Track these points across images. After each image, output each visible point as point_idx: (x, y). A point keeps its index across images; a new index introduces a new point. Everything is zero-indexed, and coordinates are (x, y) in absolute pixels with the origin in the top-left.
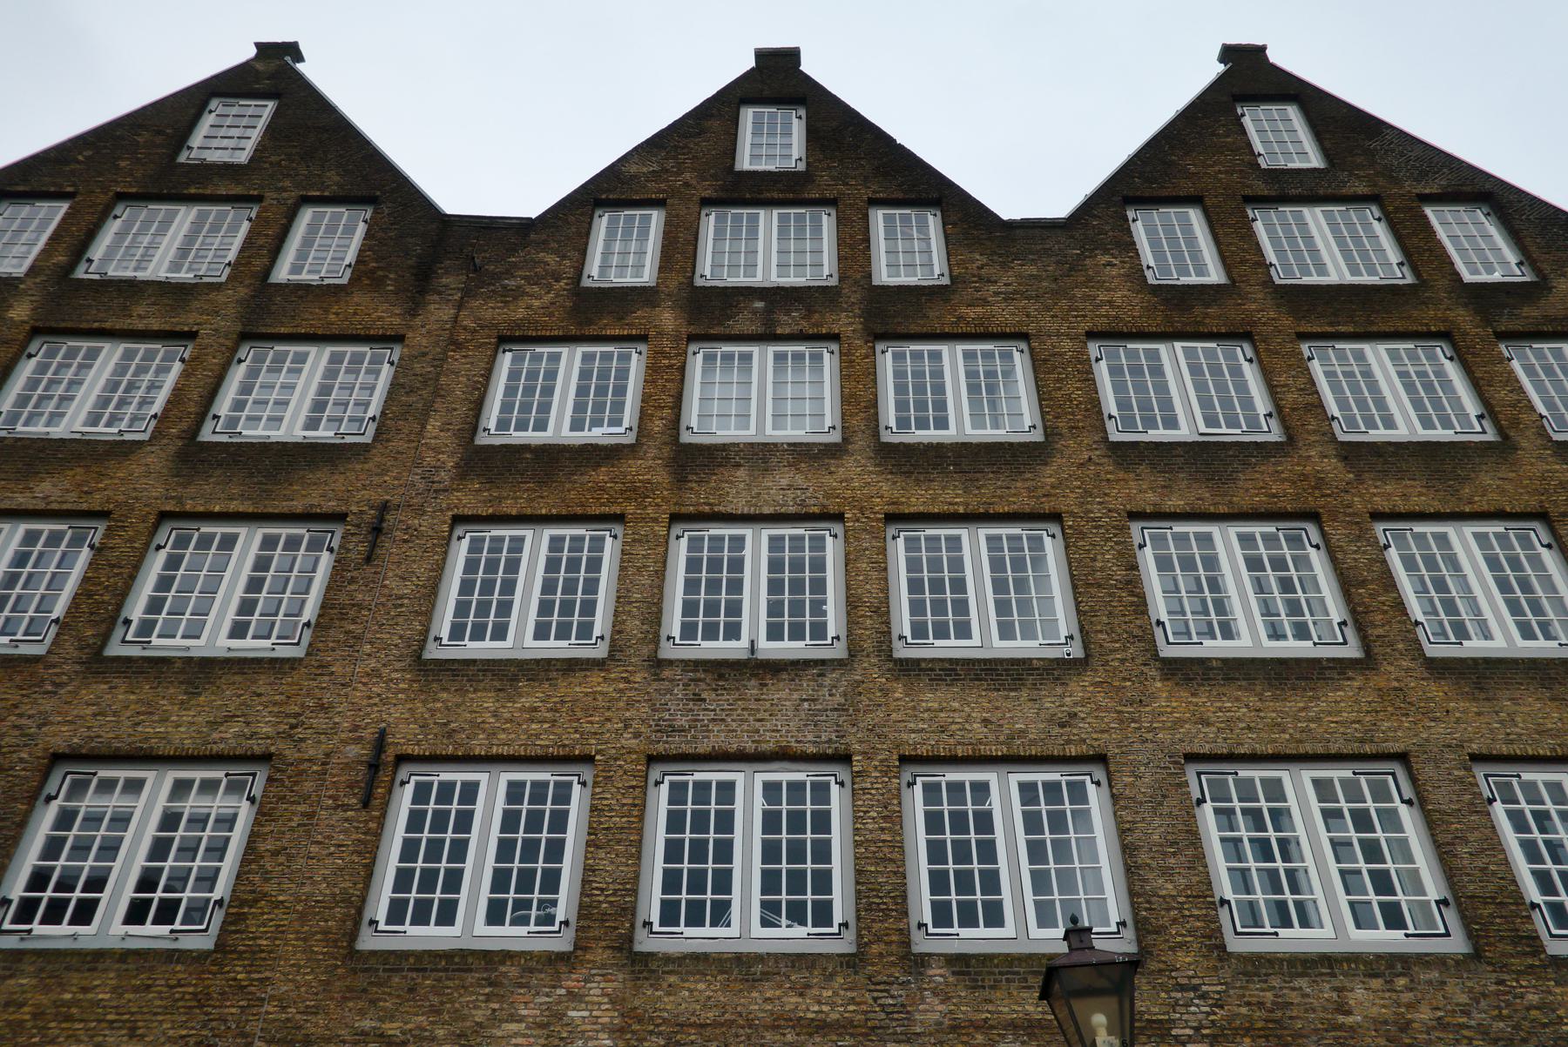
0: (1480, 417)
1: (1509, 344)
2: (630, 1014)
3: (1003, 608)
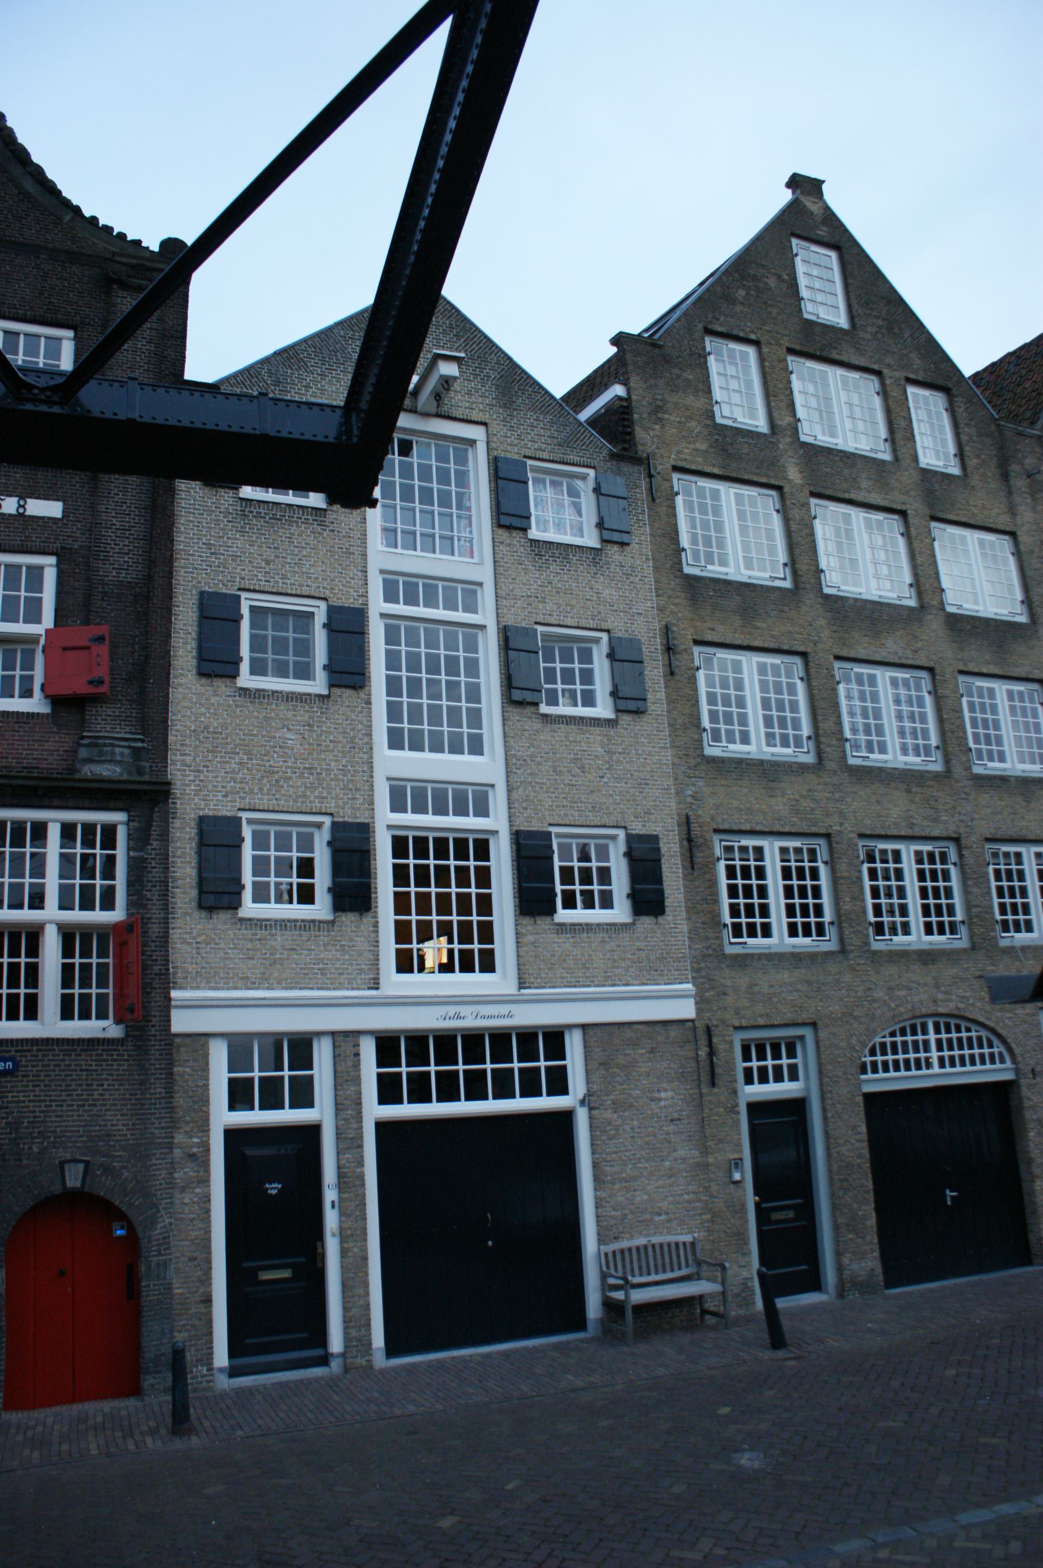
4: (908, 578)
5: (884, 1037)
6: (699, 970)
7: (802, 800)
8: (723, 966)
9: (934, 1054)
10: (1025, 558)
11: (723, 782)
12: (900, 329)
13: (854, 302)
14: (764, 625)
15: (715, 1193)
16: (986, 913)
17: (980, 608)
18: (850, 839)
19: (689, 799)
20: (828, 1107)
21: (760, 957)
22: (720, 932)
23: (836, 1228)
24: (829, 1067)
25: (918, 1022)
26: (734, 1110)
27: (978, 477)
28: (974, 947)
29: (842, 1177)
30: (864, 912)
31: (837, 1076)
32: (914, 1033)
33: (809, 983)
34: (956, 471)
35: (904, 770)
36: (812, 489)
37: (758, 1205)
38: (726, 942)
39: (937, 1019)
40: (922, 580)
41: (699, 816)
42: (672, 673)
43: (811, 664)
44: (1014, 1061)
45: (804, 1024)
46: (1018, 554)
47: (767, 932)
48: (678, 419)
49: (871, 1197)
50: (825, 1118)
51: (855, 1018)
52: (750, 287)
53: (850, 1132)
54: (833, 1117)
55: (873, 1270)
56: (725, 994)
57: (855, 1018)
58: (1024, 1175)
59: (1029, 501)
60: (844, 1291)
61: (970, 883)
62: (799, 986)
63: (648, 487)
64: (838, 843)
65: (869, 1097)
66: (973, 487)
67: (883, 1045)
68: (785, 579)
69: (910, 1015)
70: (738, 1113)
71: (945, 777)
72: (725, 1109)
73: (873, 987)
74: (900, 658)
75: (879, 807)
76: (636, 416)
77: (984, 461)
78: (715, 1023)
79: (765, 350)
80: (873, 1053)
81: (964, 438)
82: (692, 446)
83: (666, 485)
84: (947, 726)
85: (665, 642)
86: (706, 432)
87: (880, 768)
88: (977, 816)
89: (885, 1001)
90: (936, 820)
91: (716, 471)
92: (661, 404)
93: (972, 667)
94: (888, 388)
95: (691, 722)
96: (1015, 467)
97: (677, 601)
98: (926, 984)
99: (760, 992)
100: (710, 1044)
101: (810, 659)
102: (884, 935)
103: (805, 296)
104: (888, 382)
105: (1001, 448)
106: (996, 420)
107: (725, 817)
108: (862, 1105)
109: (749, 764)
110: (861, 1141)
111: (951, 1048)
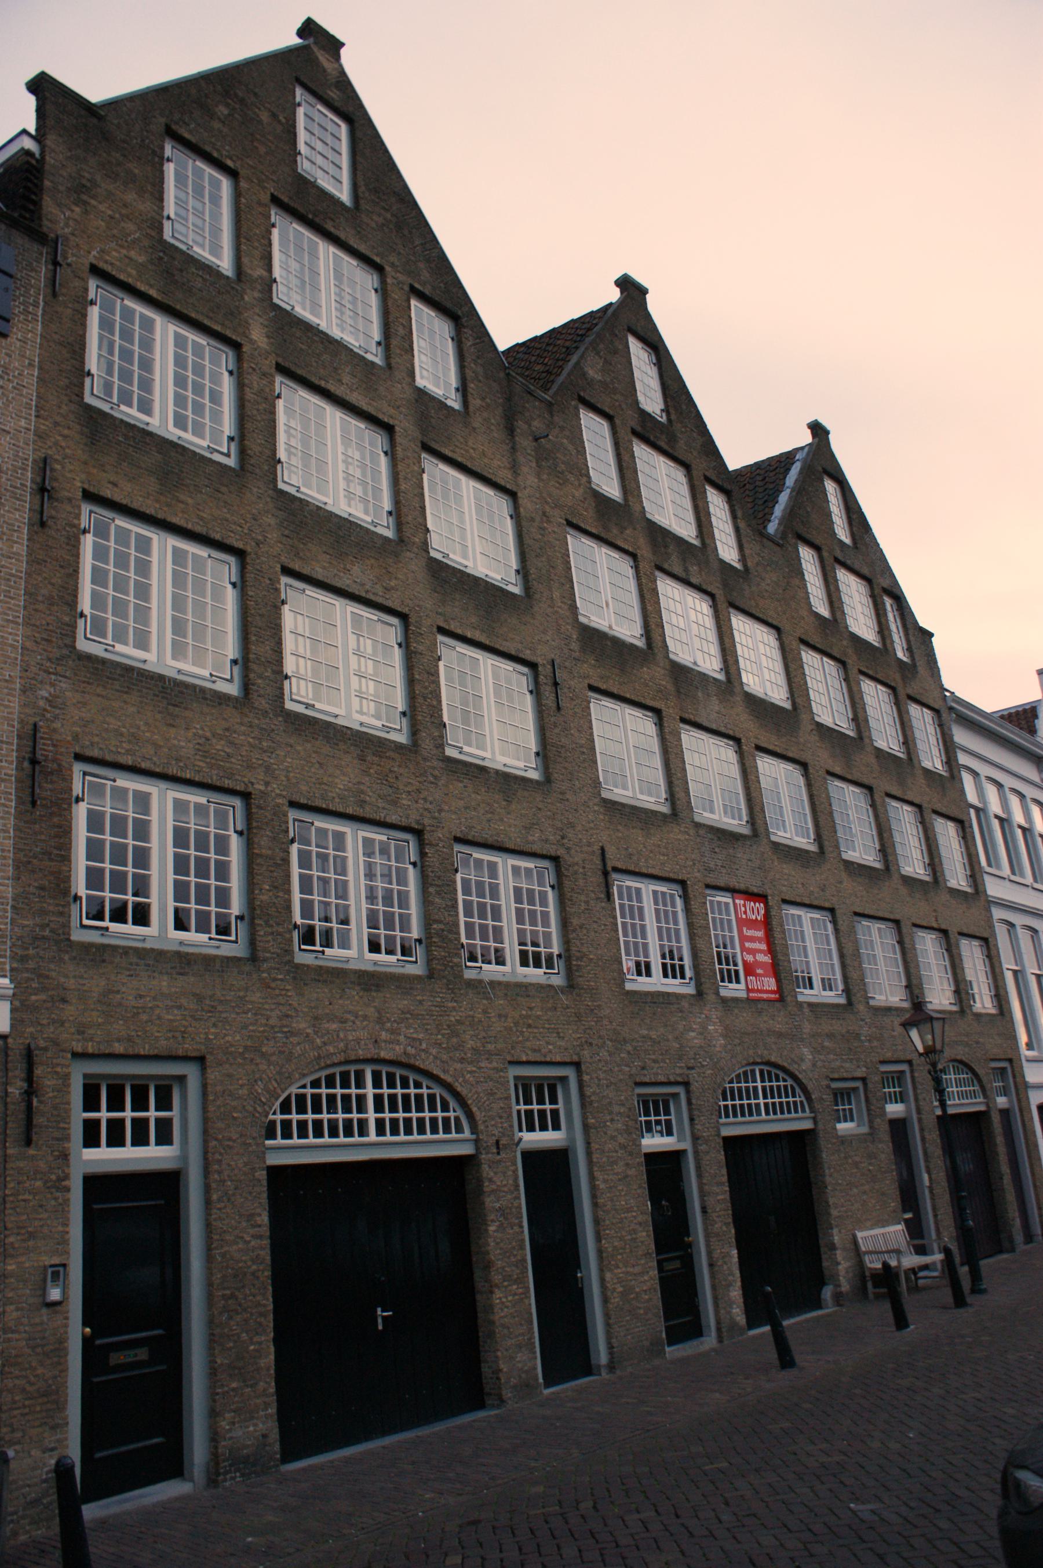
0: (231, 439)
1: (284, 380)
2: (726, 1028)
3: (179, 627)
4: (387, 505)
5: (304, 1087)
6: (24, 959)
7: (214, 741)
8: (66, 957)
9: (371, 1116)
10: (524, 523)
11: (99, 690)
12: (410, 233)
13: (361, 183)
14: (190, 501)
15: (12, 1324)
16: (450, 931)
17: (470, 564)
18: (278, 805)
19: (41, 703)
20: (214, 1185)
21: (126, 951)
22: (68, 904)
23: (213, 1372)
24: (220, 1125)
25: (352, 1068)
26: (60, 1185)
27: (480, 419)
28: (431, 975)
29: (228, 1292)
30: (288, 908)
31: (230, 1139)
32: (345, 1084)
33: (199, 998)
34: (456, 405)
35: (358, 731)
36: (280, 360)
37: (87, 1341)
38: (75, 922)
39: (377, 1067)
40: (404, 510)
41: (55, 730)
42: (43, 524)
43: (249, 567)
44: (474, 1129)
45: (185, 1058)
46: (516, 516)
47: (142, 917)
48: (110, 212)
49: (269, 1322)
50: (208, 1203)
51: (263, 1055)
52: (234, 109)
53: (244, 1224)
54: (219, 1200)
55: (264, 1436)
56: (64, 1000)
57: (263, 1055)
58: (480, 1284)
59: (534, 465)
60: (218, 1474)
61: (431, 890)
62: (184, 1001)
63: (49, 275)
64: (259, 807)
65: (275, 1172)
66: (474, 429)
67: (301, 1099)
68: (228, 455)
69: (341, 1057)
70: (68, 1189)
71: (410, 750)
72: (46, 1182)
73: (291, 1013)
74: (367, 592)
75: (321, 771)
76: (47, 183)
77: (488, 405)
78: (42, 1044)
79: (243, 184)
80: (285, 1108)
81: (469, 374)
82: (124, 252)
83: (77, 283)
84: (418, 689)
85: (39, 479)
86: (146, 243)
87: (329, 724)
88: (446, 808)
89: (308, 1035)
90: (395, 803)
91: (153, 293)
92: (88, 184)
93: (453, 627)
94: (389, 288)
95: (61, 598)
96: (520, 425)
97: (66, 432)
98: (365, 1017)
99: (120, 1004)
100: (30, 1078)
101: (248, 560)
102: (314, 944)
103: (302, 152)
104: (389, 281)
105: (509, 399)
106: (506, 368)
107: (96, 739)
108: (265, 1183)
109: (142, 675)
110: (260, 1237)
111: (393, 1109)
